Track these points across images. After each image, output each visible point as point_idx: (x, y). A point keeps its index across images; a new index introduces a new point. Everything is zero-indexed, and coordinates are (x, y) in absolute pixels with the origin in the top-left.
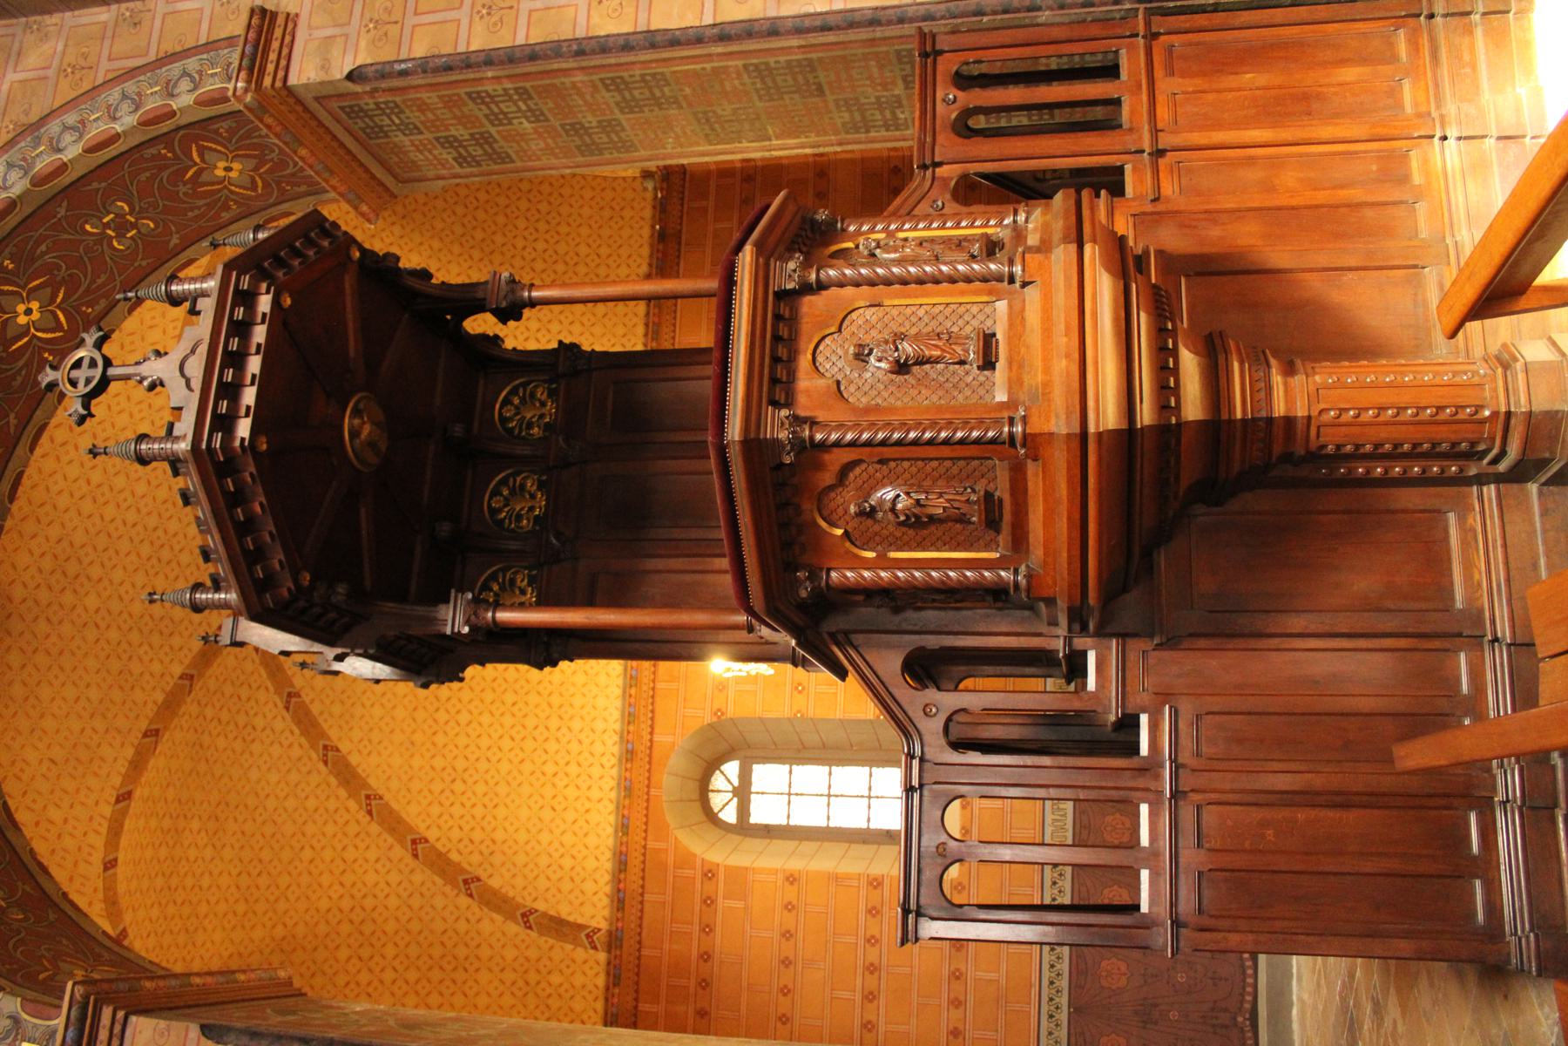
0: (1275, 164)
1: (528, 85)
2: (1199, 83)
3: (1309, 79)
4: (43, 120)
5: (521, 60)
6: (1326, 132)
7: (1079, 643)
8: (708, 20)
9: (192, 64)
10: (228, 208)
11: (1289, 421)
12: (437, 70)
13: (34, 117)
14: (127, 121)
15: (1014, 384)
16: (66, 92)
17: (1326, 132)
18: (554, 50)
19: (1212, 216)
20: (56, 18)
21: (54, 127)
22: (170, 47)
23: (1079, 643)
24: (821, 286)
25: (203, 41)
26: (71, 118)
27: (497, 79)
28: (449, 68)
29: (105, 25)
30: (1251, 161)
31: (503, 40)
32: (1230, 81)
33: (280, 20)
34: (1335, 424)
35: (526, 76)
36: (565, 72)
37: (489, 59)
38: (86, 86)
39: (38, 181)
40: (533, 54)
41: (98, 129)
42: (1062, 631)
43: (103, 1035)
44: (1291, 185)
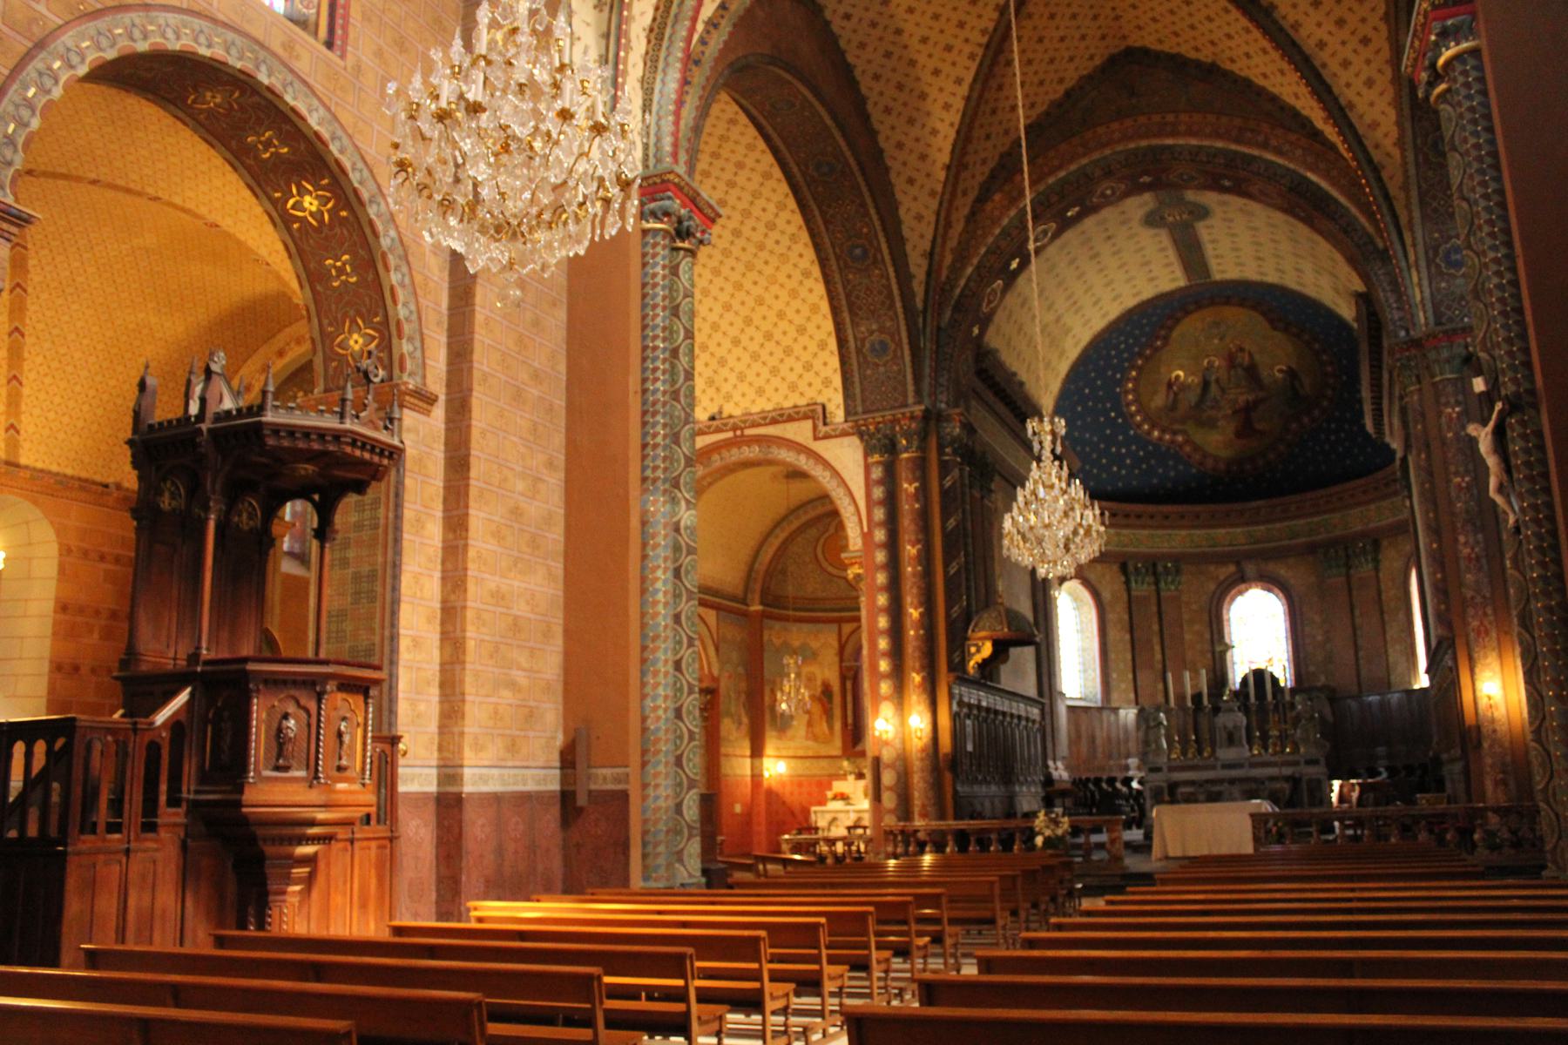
0: (345, 894)
1: (381, 530)
2: (373, 861)
3: (372, 907)
4: (408, 263)
5: (395, 534)
6: (355, 915)
7: (184, 805)
8: (402, 631)
9: (418, 354)
10: (331, 324)
11: (284, 893)
12: (397, 488)
13: (411, 258)
14: (402, 312)
15: (269, 779)
16: (418, 278)
17: (355, 915)
18: (398, 552)
19: (328, 865)
20: (447, 278)
21: (405, 269)
22: (427, 341)
23: (184, 805)
24: (366, 704)
25: (428, 361)
26: (407, 280)
27: (387, 518)
28: (397, 495)
29: (440, 306)
30: (345, 883)
31: (406, 527)
32: (373, 872)
33: (429, 407)
34: (281, 913)
35: (386, 533)
36: (385, 554)
37: (398, 517)
38: (418, 290)
39: (384, 255)
40: (398, 541)
41: (401, 295)
42: (192, 797)
43: (5, 226)
44: (337, 900)
